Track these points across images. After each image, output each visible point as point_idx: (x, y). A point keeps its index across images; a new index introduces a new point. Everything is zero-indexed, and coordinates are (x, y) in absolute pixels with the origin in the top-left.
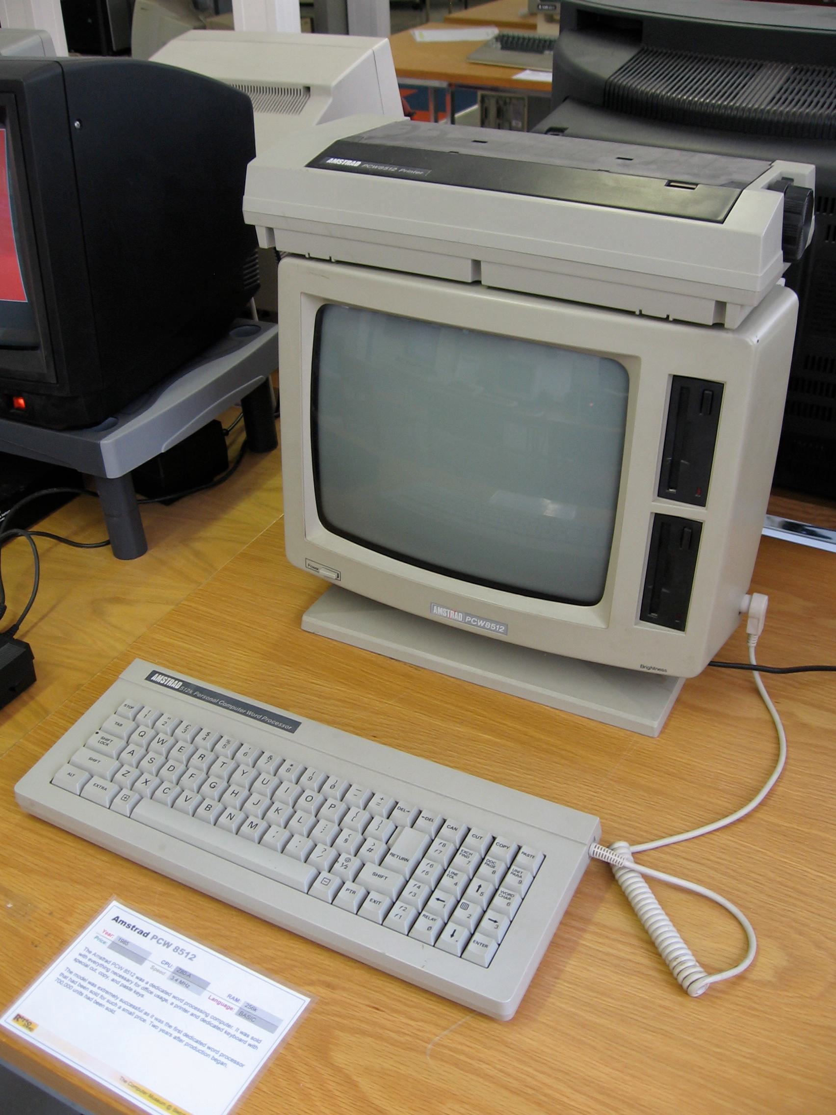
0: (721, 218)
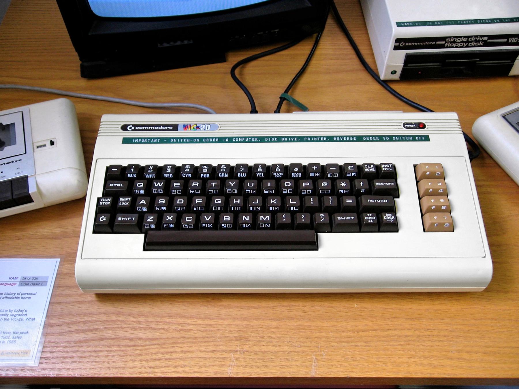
0: (237, 72)
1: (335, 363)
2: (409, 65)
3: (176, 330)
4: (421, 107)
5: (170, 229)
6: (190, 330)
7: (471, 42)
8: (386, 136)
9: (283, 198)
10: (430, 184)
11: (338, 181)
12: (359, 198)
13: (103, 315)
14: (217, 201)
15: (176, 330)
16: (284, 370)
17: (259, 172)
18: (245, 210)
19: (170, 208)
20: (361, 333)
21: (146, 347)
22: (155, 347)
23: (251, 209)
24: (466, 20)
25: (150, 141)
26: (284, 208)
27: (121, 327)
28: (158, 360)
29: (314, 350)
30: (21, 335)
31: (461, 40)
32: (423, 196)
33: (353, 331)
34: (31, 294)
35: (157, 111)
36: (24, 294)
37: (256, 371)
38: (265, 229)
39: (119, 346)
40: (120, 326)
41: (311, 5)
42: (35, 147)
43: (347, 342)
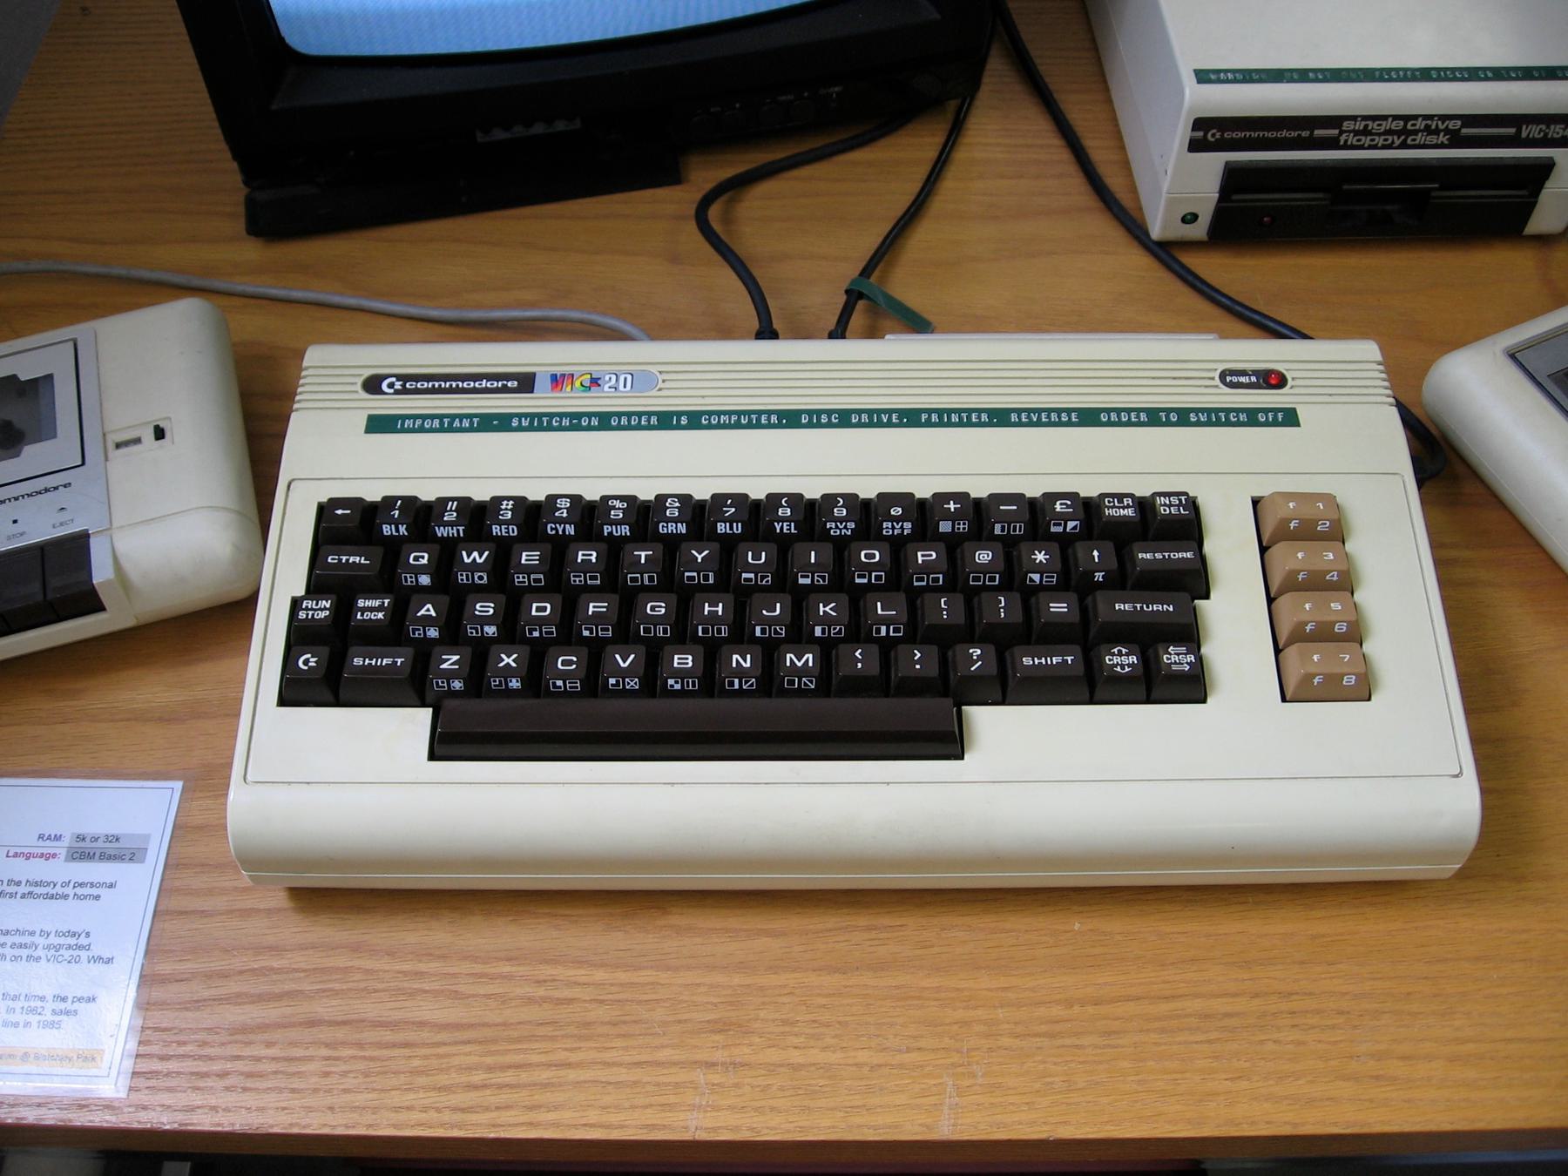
0: (714, 212)
1: (1012, 1099)
2: (1235, 197)
3: (530, 1001)
4: (1271, 324)
5: (510, 693)
6: (570, 1001)
7: (1416, 132)
8: (1168, 411)
9: (857, 600)
10: (1300, 555)
11: (1024, 547)
12: (1089, 599)
13: (311, 952)
14: (653, 609)
15: (530, 1001)
16: (858, 1120)
17: (783, 520)
18: (740, 637)
19: (511, 632)
20: (1090, 1009)
21: (442, 1050)
22: (468, 1048)
23: (758, 633)
24: (1397, 70)
25: (450, 424)
26: (858, 630)
27: (365, 989)
28: (476, 1087)
29: (949, 1061)
30: (76, 1006)
31: (1386, 125)
32: (1280, 593)
33: (1069, 1004)
34: (101, 885)
35: (472, 332)
36: (81, 885)
37: (772, 1124)
38: (802, 693)
39: (360, 1045)
40: (362, 985)
41: (938, 17)
42: (111, 446)
43: (1051, 1036)
